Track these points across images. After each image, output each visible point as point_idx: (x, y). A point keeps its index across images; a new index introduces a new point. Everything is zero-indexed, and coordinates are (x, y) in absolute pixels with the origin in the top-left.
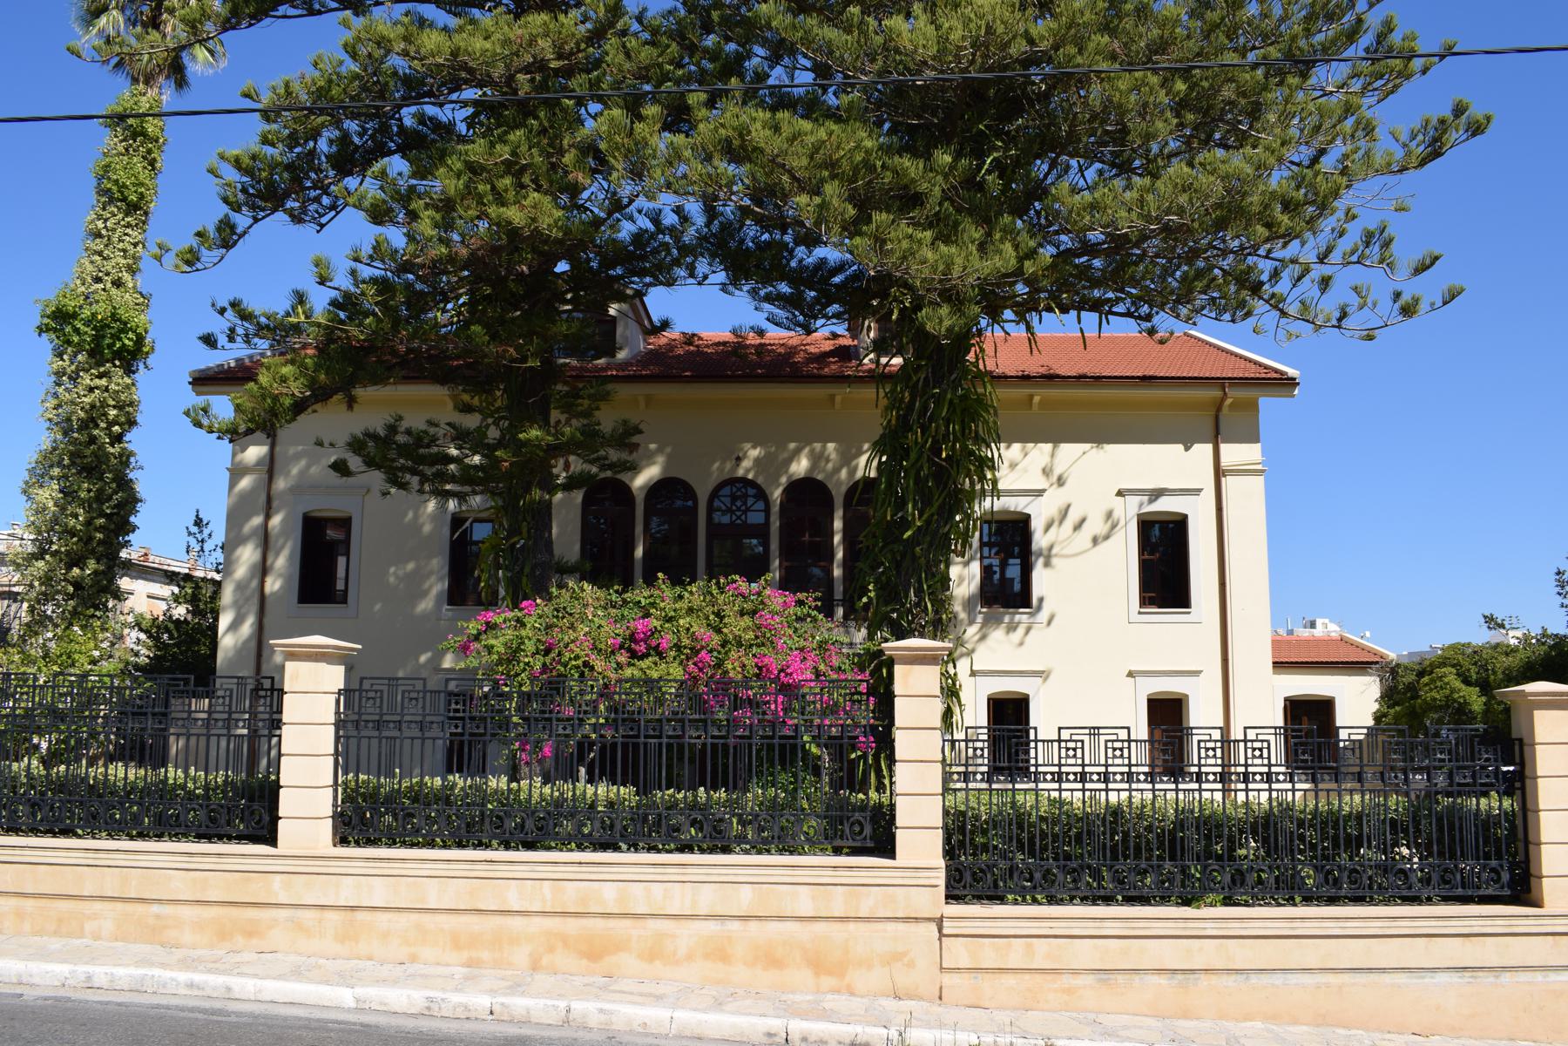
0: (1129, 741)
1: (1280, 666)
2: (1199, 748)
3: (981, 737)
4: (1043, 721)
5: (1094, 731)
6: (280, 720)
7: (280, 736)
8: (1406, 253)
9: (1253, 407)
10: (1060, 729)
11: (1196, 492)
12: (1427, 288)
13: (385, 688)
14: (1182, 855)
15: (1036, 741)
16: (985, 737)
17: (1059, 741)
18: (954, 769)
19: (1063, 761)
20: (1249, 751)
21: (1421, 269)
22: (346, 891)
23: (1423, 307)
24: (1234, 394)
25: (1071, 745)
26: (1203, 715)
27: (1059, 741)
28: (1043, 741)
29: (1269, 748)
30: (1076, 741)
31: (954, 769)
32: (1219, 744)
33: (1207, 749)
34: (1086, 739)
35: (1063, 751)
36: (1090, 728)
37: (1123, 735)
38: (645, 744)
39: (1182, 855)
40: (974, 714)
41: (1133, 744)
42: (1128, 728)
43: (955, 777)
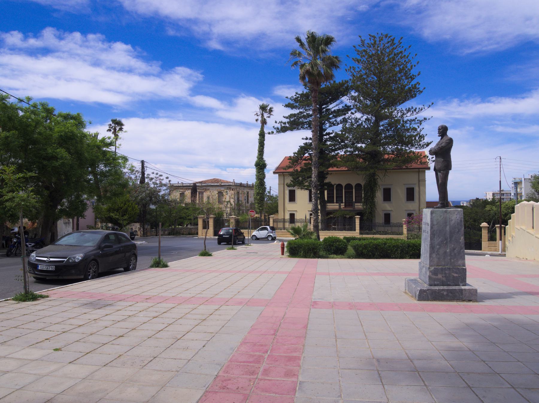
11: (416, 184)
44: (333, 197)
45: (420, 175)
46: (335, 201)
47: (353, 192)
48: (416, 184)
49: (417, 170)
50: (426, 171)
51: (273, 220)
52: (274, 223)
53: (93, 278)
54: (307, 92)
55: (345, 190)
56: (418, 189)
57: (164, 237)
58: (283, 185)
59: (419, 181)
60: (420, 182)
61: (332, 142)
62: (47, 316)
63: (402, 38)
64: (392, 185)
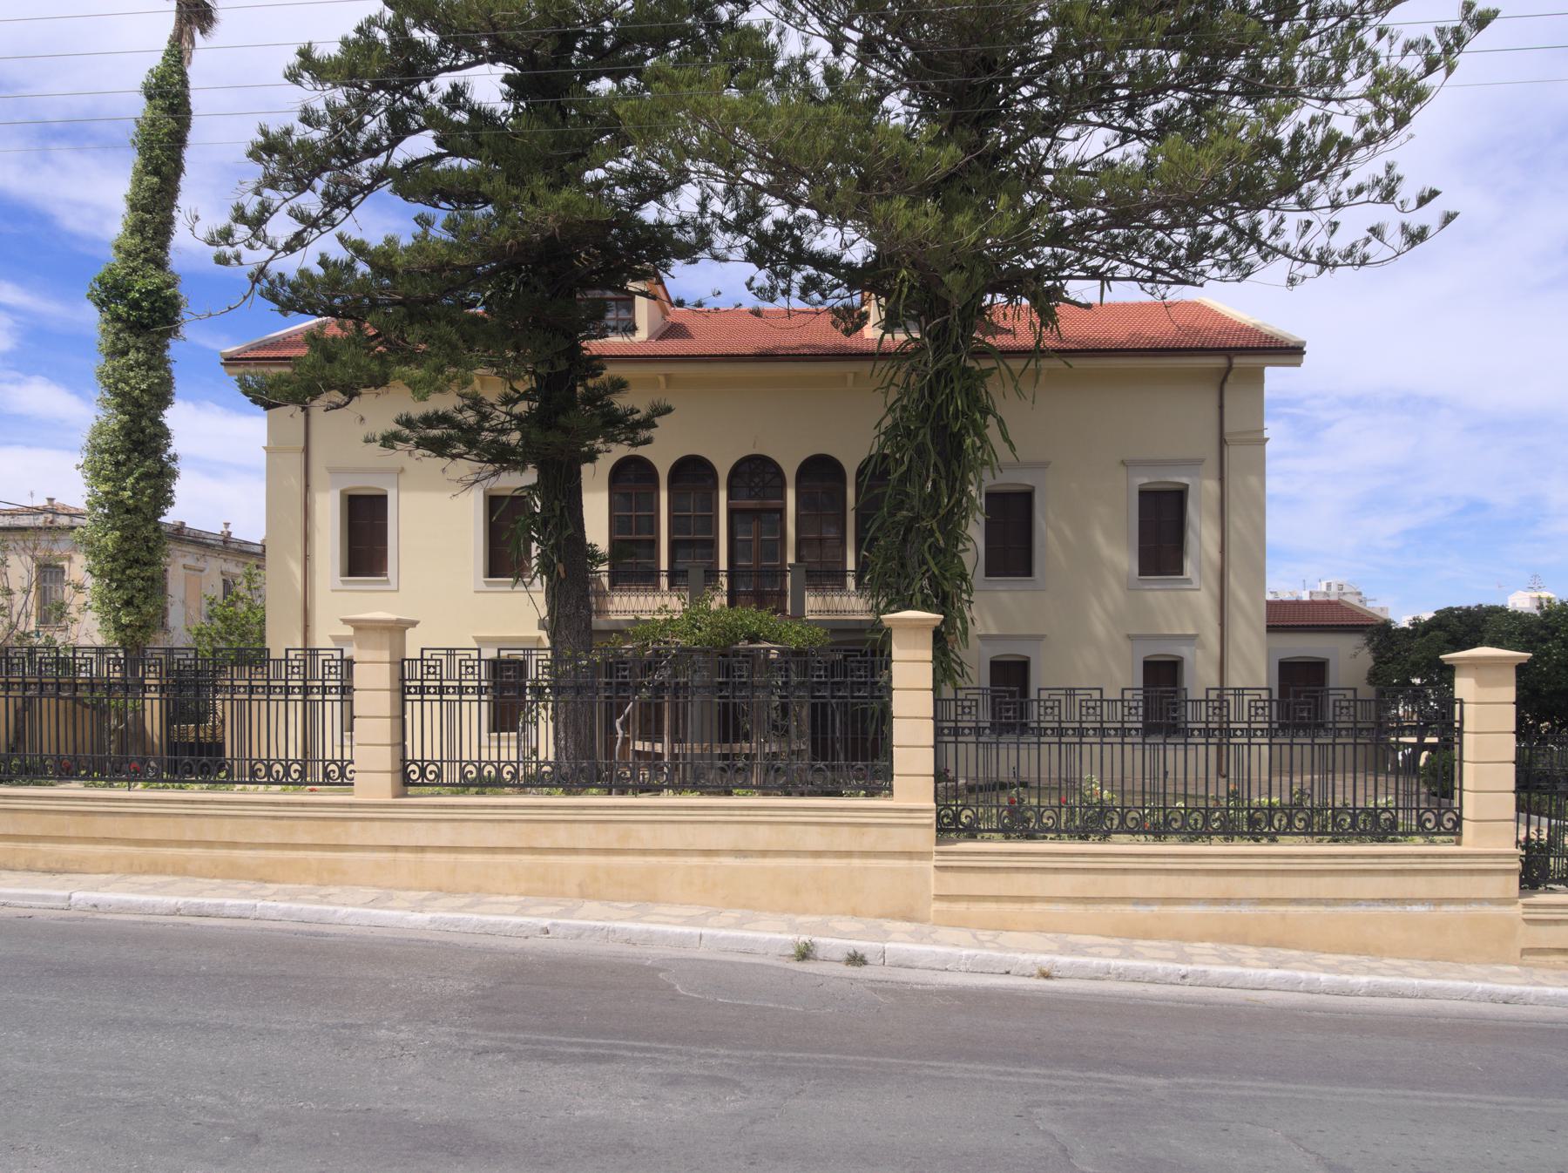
0: (1102, 700)
1: (1272, 629)
2: (460, 666)
3: (1136, 697)
4: (1040, 678)
5: (451, 652)
6: (351, 687)
7: (352, 701)
8: (1408, 192)
9: (1257, 378)
10: (422, 649)
11: (1198, 462)
12: (1429, 216)
13: (444, 658)
14: (942, 853)
15: (1186, 701)
16: (1141, 697)
17: (1122, 701)
18: (945, 724)
19: (1126, 719)
20: (425, 668)
21: (1423, 201)
22: (401, 835)
23: (1430, 233)
24: (1239, 361)
25: (967, 703)
26: (1200, 677)
27: (1122, 701)
28: (1192, 701)
29: (441, 666)
30: (1054, 701)
31: (945, 724)
32: (1141, 704)
33: (467, 667)
34: (1063, 698)
35: (425, 668)
36: (1066, 689)
37: (1096, 695)
38: (735, 704)
39: (942, 853)
40: (979, 676)
41: (1105, 704)
42: (1101, 690)
43: (946, 731)
44: (654, 544)
45: (1227, 387)
46: (666, 588)
47: (782, 511)
48: (1198, 462)
49: (1219, 362)
50: (1269, 372)
51: (400, 663)
52: (413, 709)
53: (504, 497)
54: (334, 338)
55: (730, 497)
56: (1216, 535)
57: (809, 347)
58: (298, 459)
59: (1222, 442)
60: (1232, 452)
61: (420, 388)
62: (177, 55)
63: (1434, 194)
64: (1043, 465)
